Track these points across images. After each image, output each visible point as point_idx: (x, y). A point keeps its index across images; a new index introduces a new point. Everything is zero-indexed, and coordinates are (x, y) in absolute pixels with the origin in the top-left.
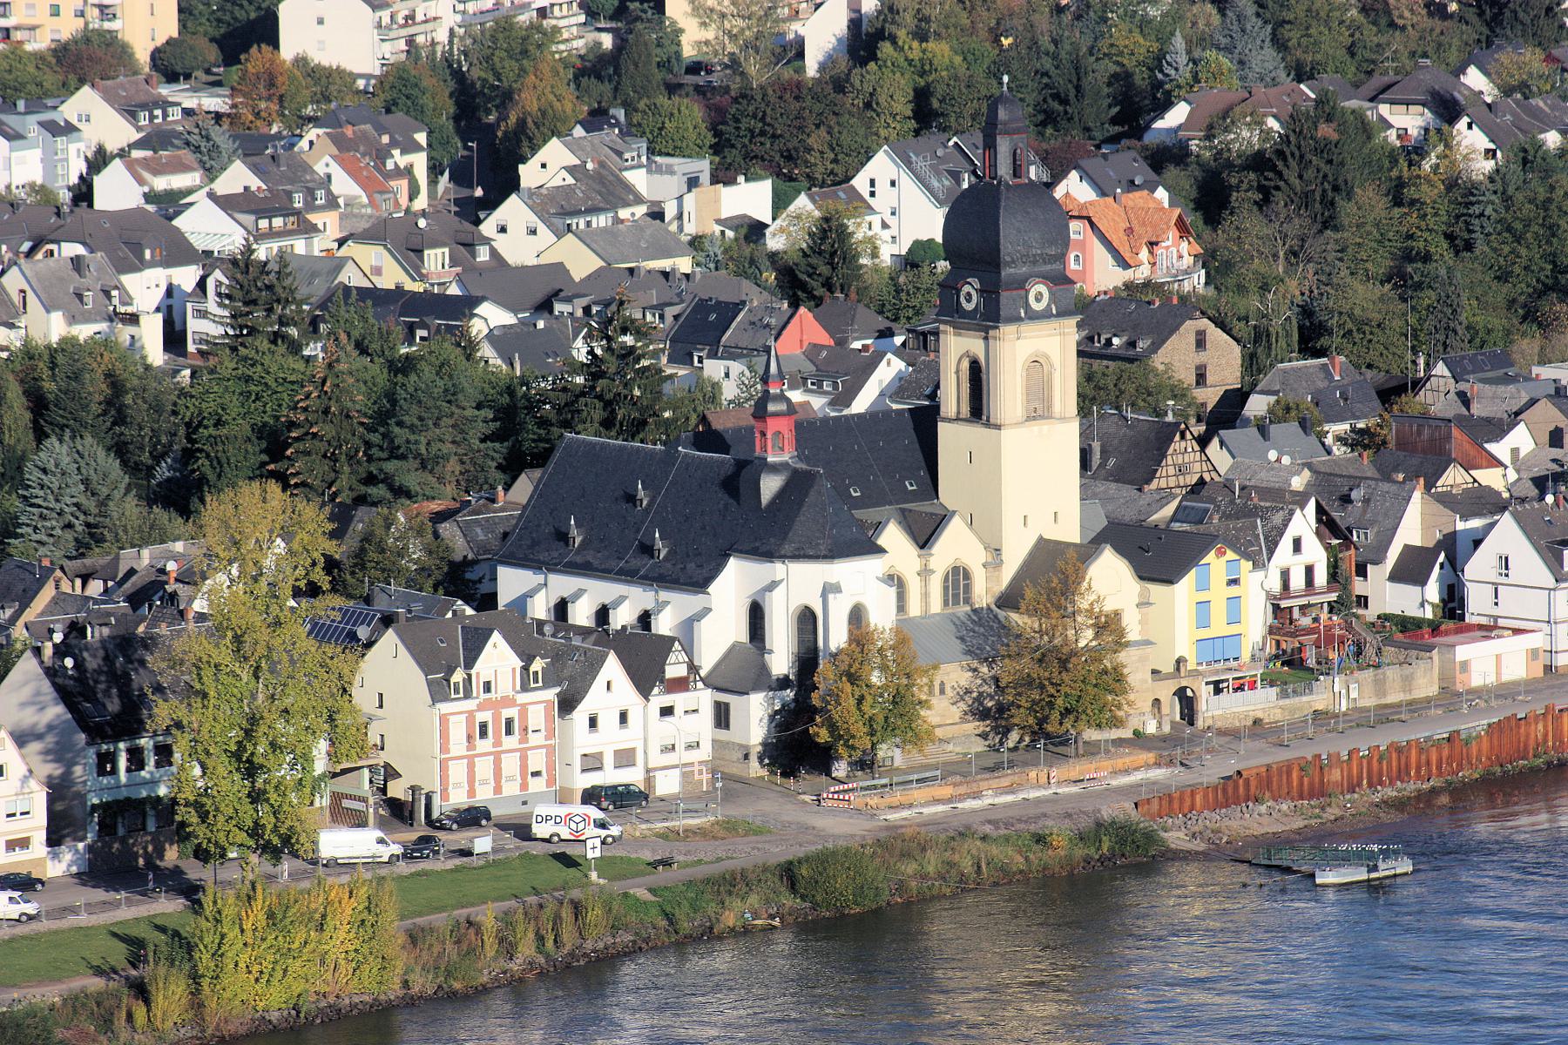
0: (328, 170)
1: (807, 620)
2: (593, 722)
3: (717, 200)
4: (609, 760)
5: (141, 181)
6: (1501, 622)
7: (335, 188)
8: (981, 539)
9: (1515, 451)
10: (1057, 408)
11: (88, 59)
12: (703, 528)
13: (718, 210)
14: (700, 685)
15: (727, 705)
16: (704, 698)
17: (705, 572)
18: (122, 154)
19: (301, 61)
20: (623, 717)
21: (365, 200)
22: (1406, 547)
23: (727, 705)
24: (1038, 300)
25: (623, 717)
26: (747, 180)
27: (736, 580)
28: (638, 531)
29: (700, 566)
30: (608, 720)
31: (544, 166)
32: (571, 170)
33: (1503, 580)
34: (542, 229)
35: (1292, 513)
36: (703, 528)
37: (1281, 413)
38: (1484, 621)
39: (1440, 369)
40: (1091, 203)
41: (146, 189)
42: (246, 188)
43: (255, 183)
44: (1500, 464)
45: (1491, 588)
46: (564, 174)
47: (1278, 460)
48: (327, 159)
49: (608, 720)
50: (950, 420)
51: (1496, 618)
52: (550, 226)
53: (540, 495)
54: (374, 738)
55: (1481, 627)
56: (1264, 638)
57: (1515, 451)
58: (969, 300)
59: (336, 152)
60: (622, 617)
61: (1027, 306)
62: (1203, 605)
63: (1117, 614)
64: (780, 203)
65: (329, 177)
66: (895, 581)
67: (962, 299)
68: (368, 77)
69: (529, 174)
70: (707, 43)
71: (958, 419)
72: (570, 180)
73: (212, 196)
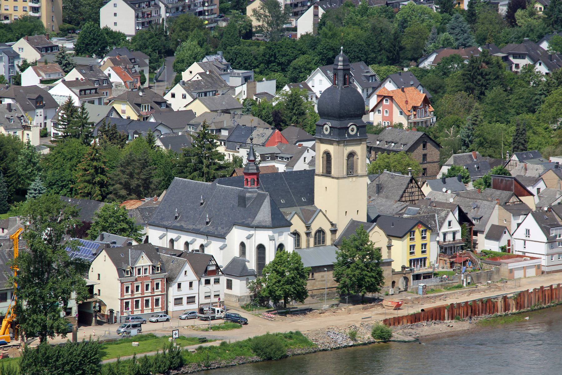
0: (109, 72)
1: (261, 248)
2: (179, 286)
3: (255, 87)
4: (185, 301)
5: (39, 75)
6: (527, 254)
7: (111, 80)
8: (368, 211)
9: (539, 189)
10: (360, 172)
11: (27, 28)
12: (225, 214)
13: (255, 91)
14: (220, 273)
15: (231, 281)
16: (223, 279)
17: (224, 231)
18: (34, 64)
19: (106, 29)
20: (191, 284)
21: (123, 84)
22: (493, 225)
23: (231, 281)
24: (352, 131)
25: (191, 284)
26: (267, 80)
27: (237, 235)
28: (200, 214)
29: (223, 228)
30: (185, 285)
31: (191, 72)
32: (200, 74)
33: (527, 238)
34: (188, 96)
35: (448, 212)
36: (225, 214)
37: (452, 173)
38: (521, 254)
39: (515, 157)
40: (393, 91)
41: (41, 78)
42: (77, 79)
43: (80, 77)
44: (531, 194)
45: (523, 242)
46: (198, 76)
47: (446, 192)
48: (109, 68)
49: (185, 285)
50: (319, 175)
51: (524, 253)
52: (191, 95)
53: (165, 200)
54: (95, 291)
55: (518, 256)
56: (437, 258)
57: (539, 189)
58: (327, 130)
59: (113, 65)
60: (195, 246)
61: (349, 134)
62: (412, 247)
63: (380, 249)
64: (279, 87)
65: (109, 75)
66: (296, 234)
67: (324, 131)
68: (129, 36)
69: (186, 76)
70: (259, 26)
71: (322, 175)
72: (200, 78)
73: (64, 81)
